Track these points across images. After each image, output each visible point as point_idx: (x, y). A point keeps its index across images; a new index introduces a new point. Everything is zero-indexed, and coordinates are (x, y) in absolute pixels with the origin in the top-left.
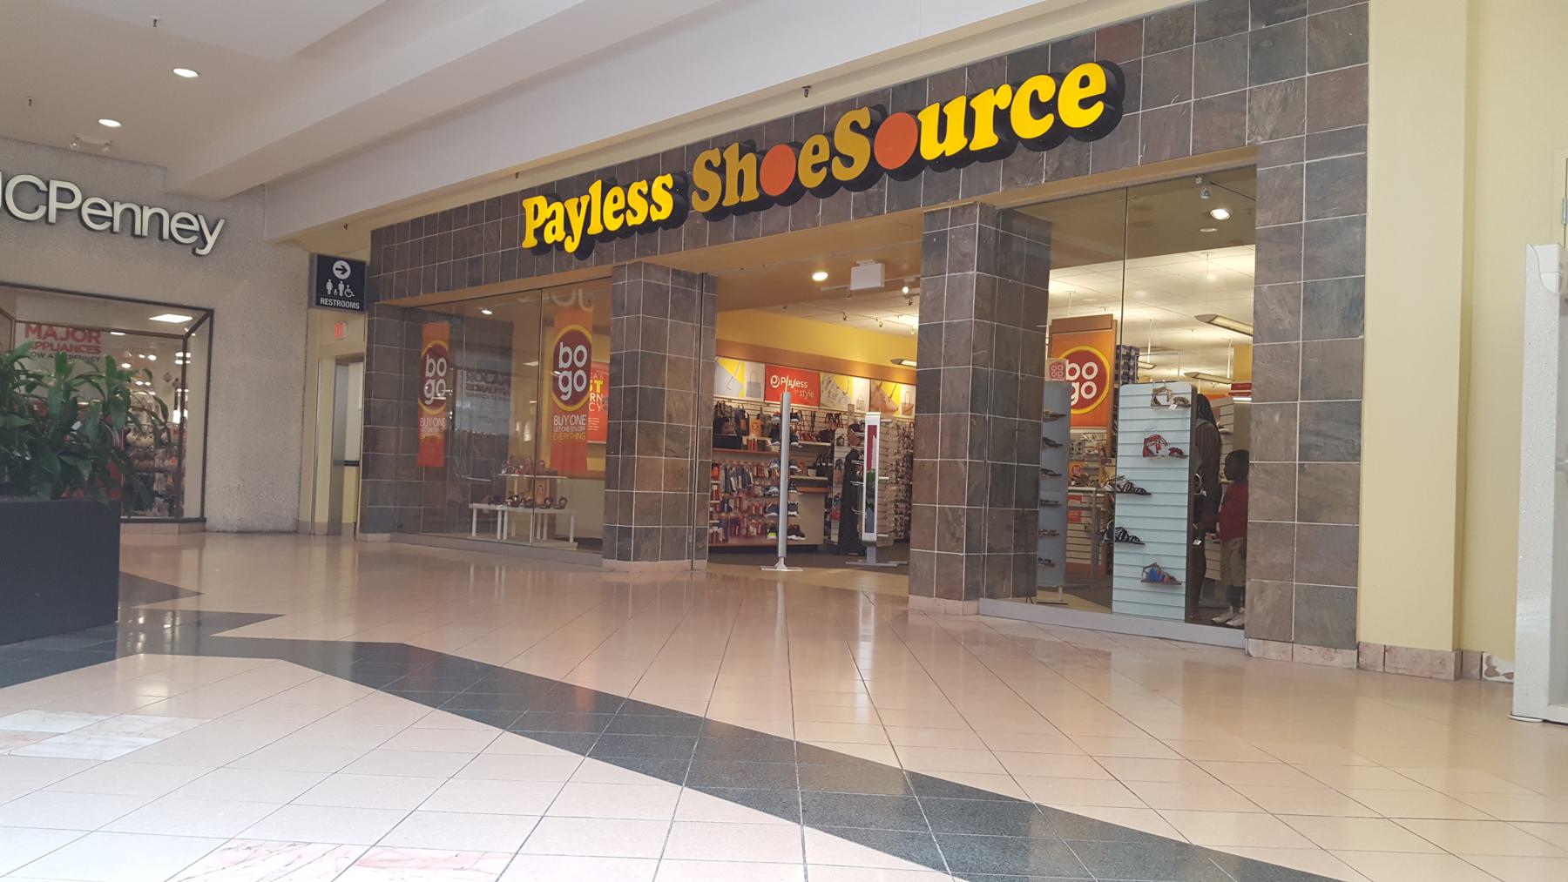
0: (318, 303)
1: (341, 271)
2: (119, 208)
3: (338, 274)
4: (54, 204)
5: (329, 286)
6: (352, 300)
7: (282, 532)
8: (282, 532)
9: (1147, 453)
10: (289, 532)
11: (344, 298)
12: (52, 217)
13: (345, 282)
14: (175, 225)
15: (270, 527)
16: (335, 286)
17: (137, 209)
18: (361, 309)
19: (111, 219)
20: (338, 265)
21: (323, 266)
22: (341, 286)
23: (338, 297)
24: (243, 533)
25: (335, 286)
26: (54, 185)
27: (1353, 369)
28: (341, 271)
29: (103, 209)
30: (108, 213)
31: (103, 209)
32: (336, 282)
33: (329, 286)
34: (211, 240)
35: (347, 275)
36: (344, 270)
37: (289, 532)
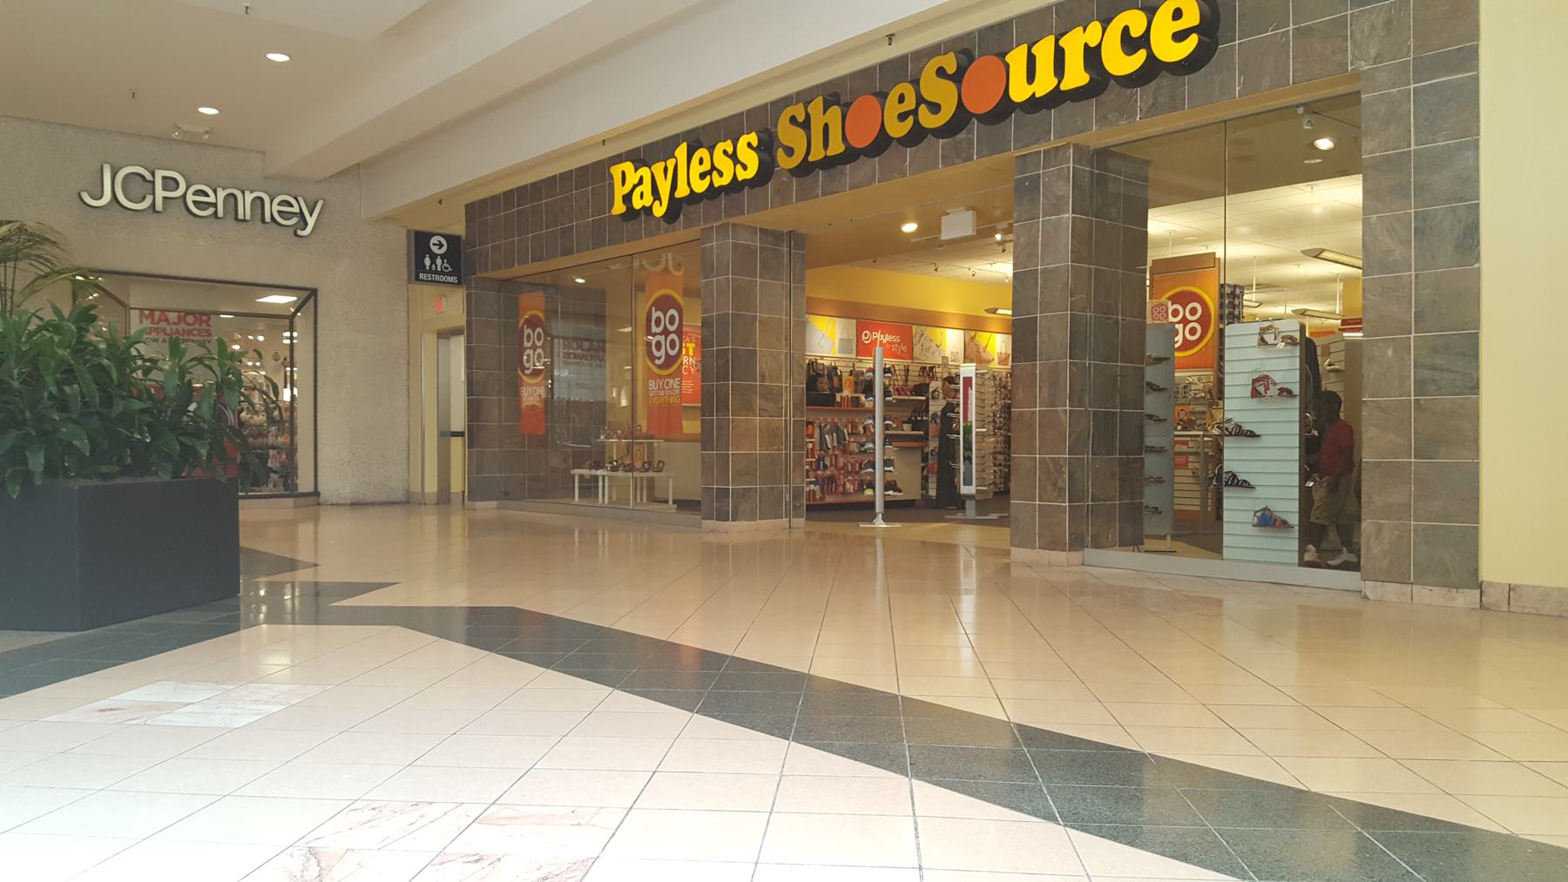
1: (438, 246)
2: (222, 194)
3: (435, 249)
4: (160, 193)
5: (427, 261)
6: (449, 274)
7: (394, 503)
8: (394, 503)
9: (1255, 394)
11: (442, 273)
12: (159, 206)
13: (442, 257)
14: (276, 208)
15: (382, 498)
16: (433, 261)
18: (459, 283)
19: (215, 205)
20: (434, 240)
21: (420, 241)
22: (439, 261)
23: (436, 272)
24: (356, 505)
25: (433, 261)
26: (159, 174)
28: (438, 246)
29: (207, 195)
30: (211, 199)
31: (207, 195)
32: (433, 257)
33: (427, 261)
34: (311, 221)
36: (441, 245)
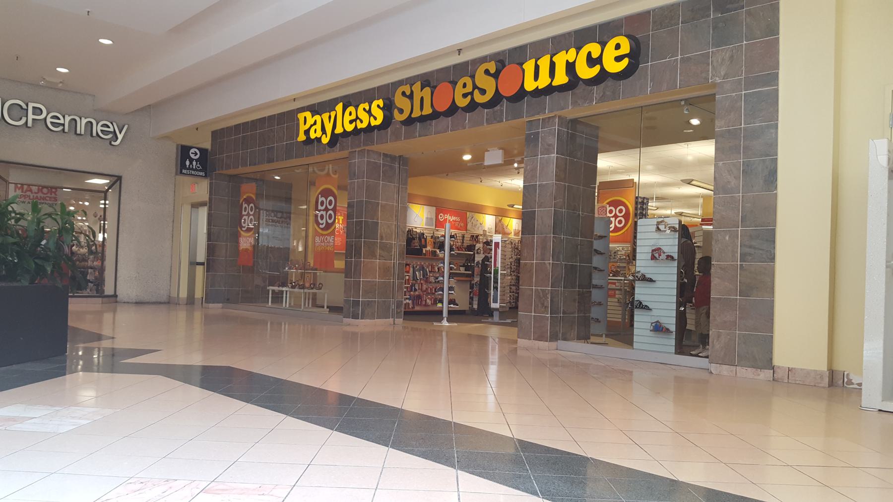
0: (181, 172)
1: (194, 154)
2: (68, 119)
3: (192, 156)
4: (31, 116)
5: (188, 163)
6: (200, 171)
7: (160, 303)
8: (160, 303)
10: (164, 303)
11: (196, 170)
12: (30, 124)
13: (197, 160)
14: (99, 128)
15: (154, 300)
16: (191, 163)
17: (78, 119)
18: (206, 176)
19: (63, 125)
20: (192, 151)
21: (184, 151)
22: (194, 163)
23: (192, 169)
24: (139, 303)
25: (191, 163)
26: (31, 105)
27: (770, 210)
28: (194, 154)
29: (59, 119)
30: (61, 121)
31: (59, 119)
32: (191, 160)
33: (188, 163)
34: (120, 137)
35: (198, 156)
36: (196, 154)
37: (164, 303)
